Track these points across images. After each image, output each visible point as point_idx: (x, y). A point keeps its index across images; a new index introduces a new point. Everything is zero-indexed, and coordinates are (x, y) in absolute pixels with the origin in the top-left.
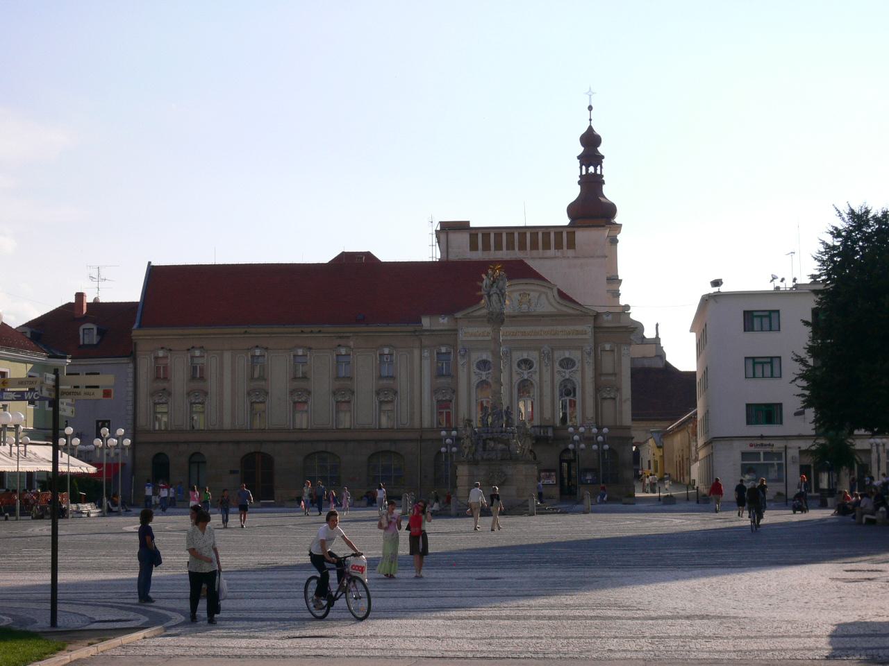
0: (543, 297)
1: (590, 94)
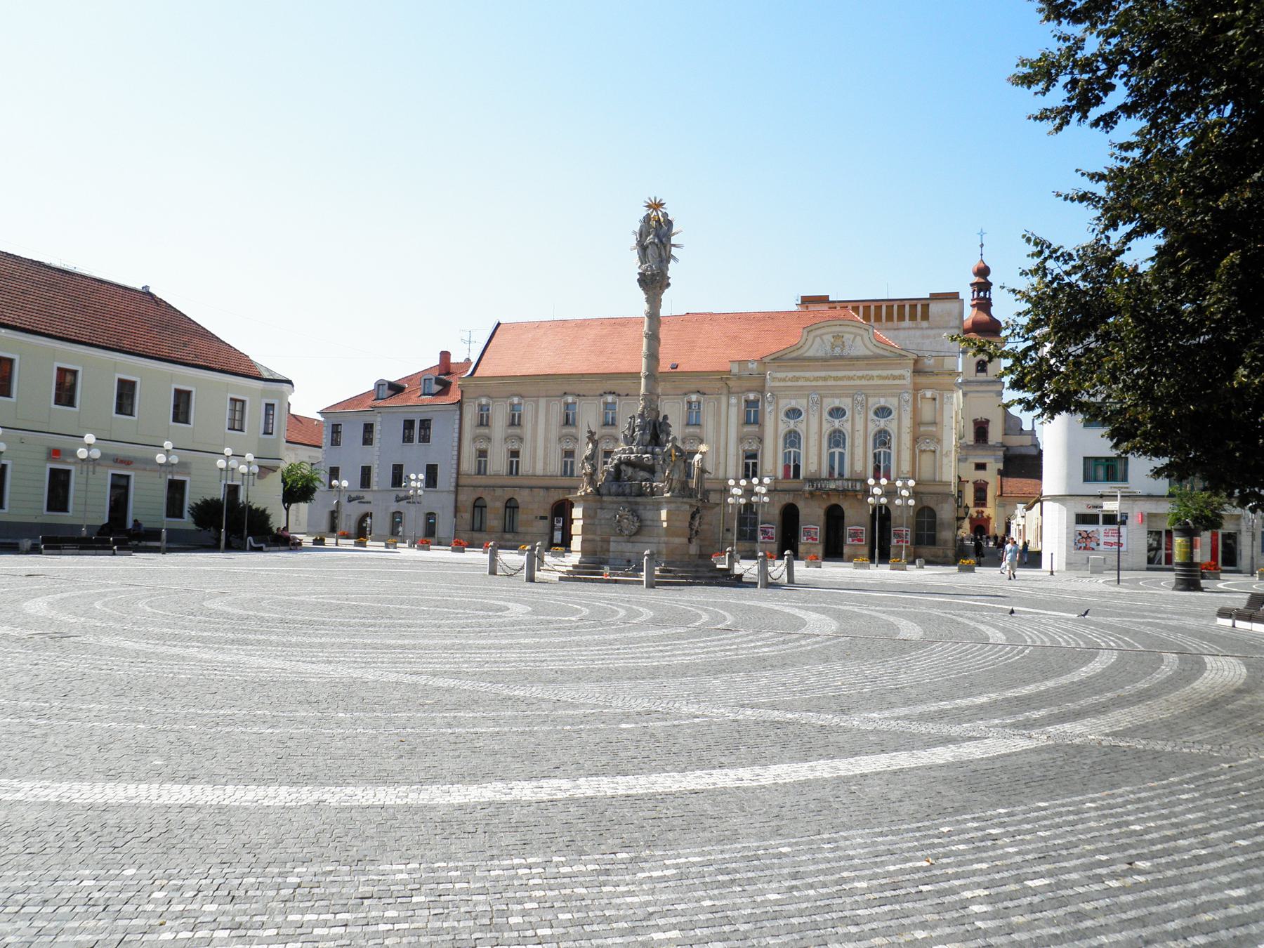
0: (858, 338)
1: (982, 234)
